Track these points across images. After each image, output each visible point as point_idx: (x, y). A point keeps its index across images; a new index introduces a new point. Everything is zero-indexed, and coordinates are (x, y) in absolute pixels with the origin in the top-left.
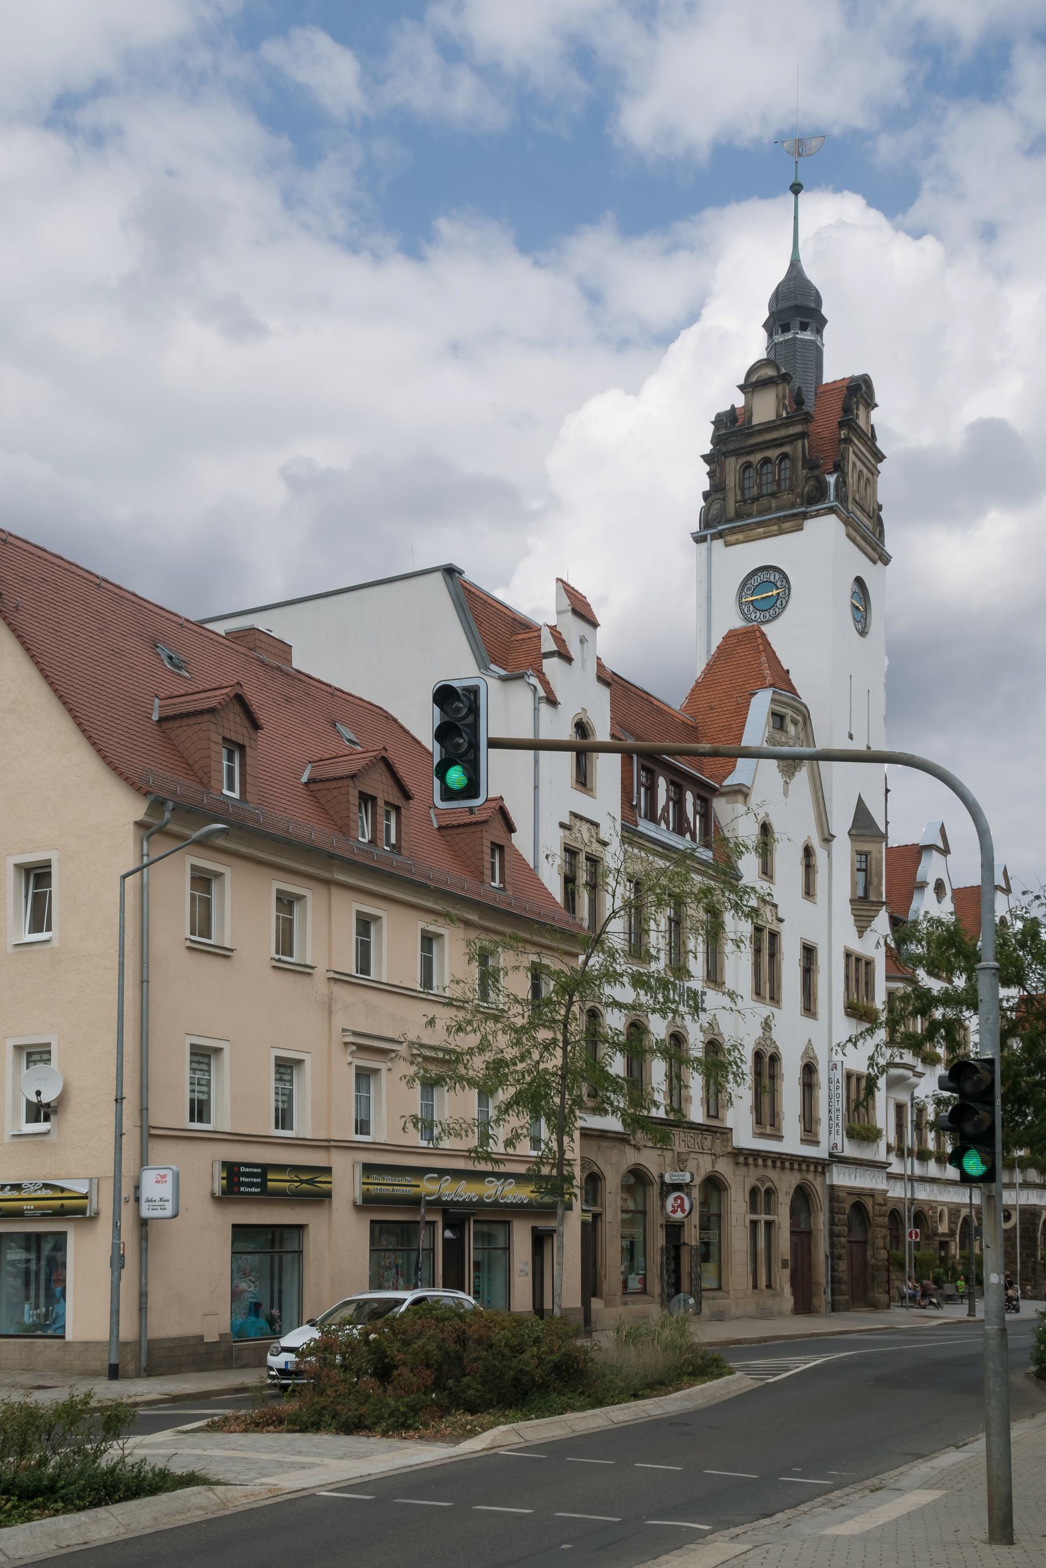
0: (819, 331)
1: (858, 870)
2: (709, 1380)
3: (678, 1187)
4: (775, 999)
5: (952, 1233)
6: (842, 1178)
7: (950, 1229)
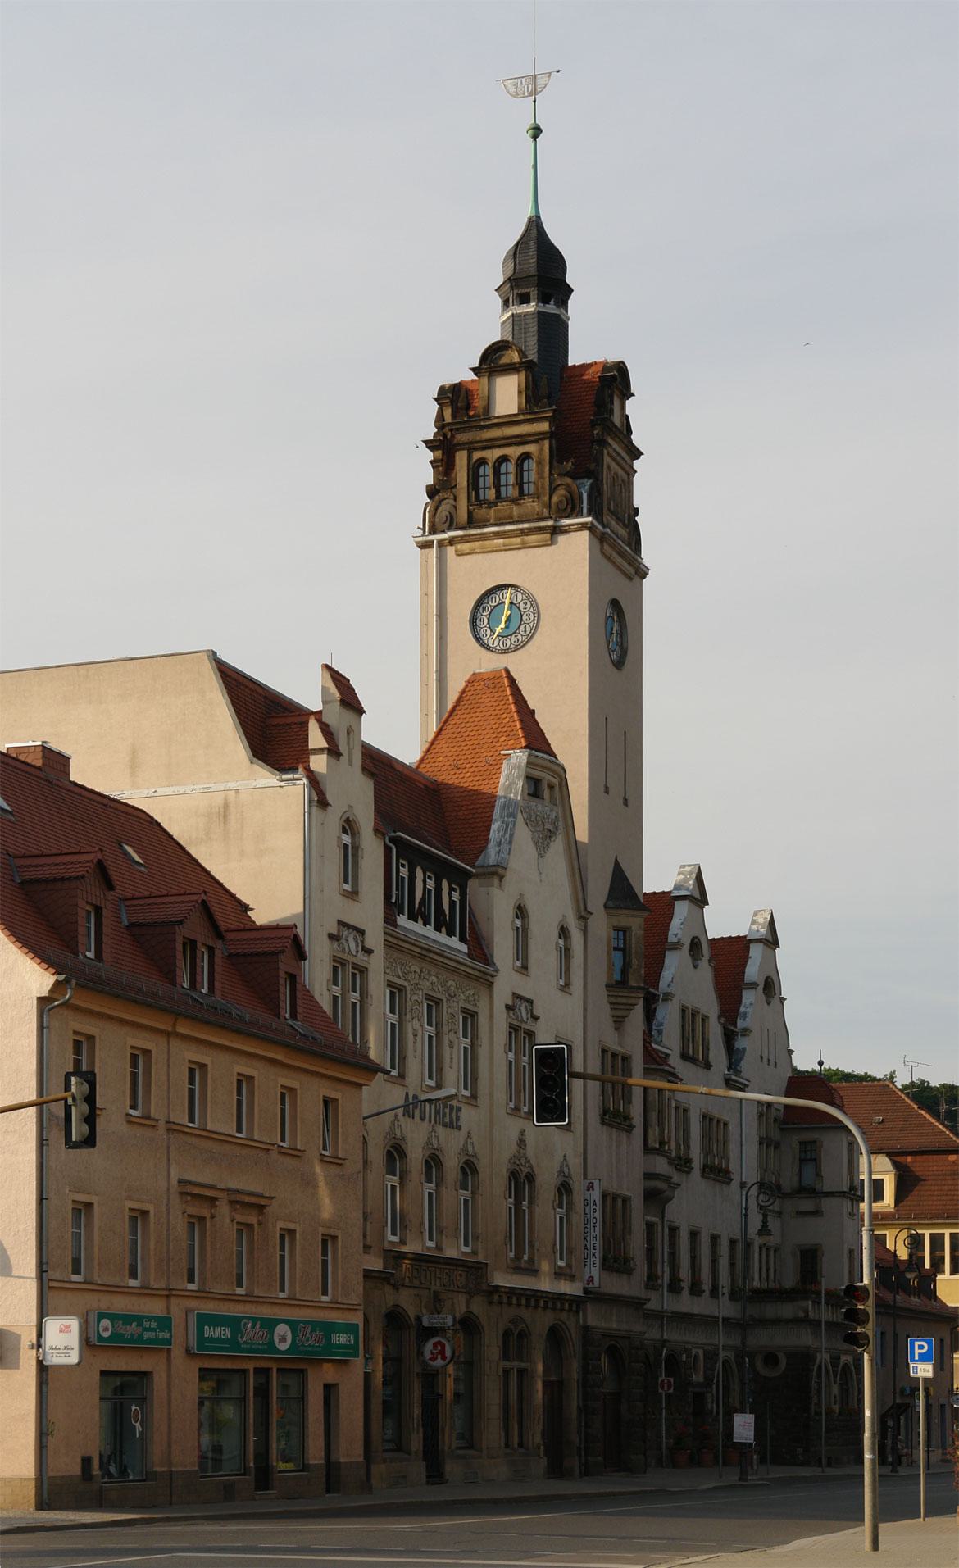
0: (564, 303)
1: (615, 949)
3: (432, 1332)
5: (708, 1381)
6: (593, 1317)
7: (705, 1378)
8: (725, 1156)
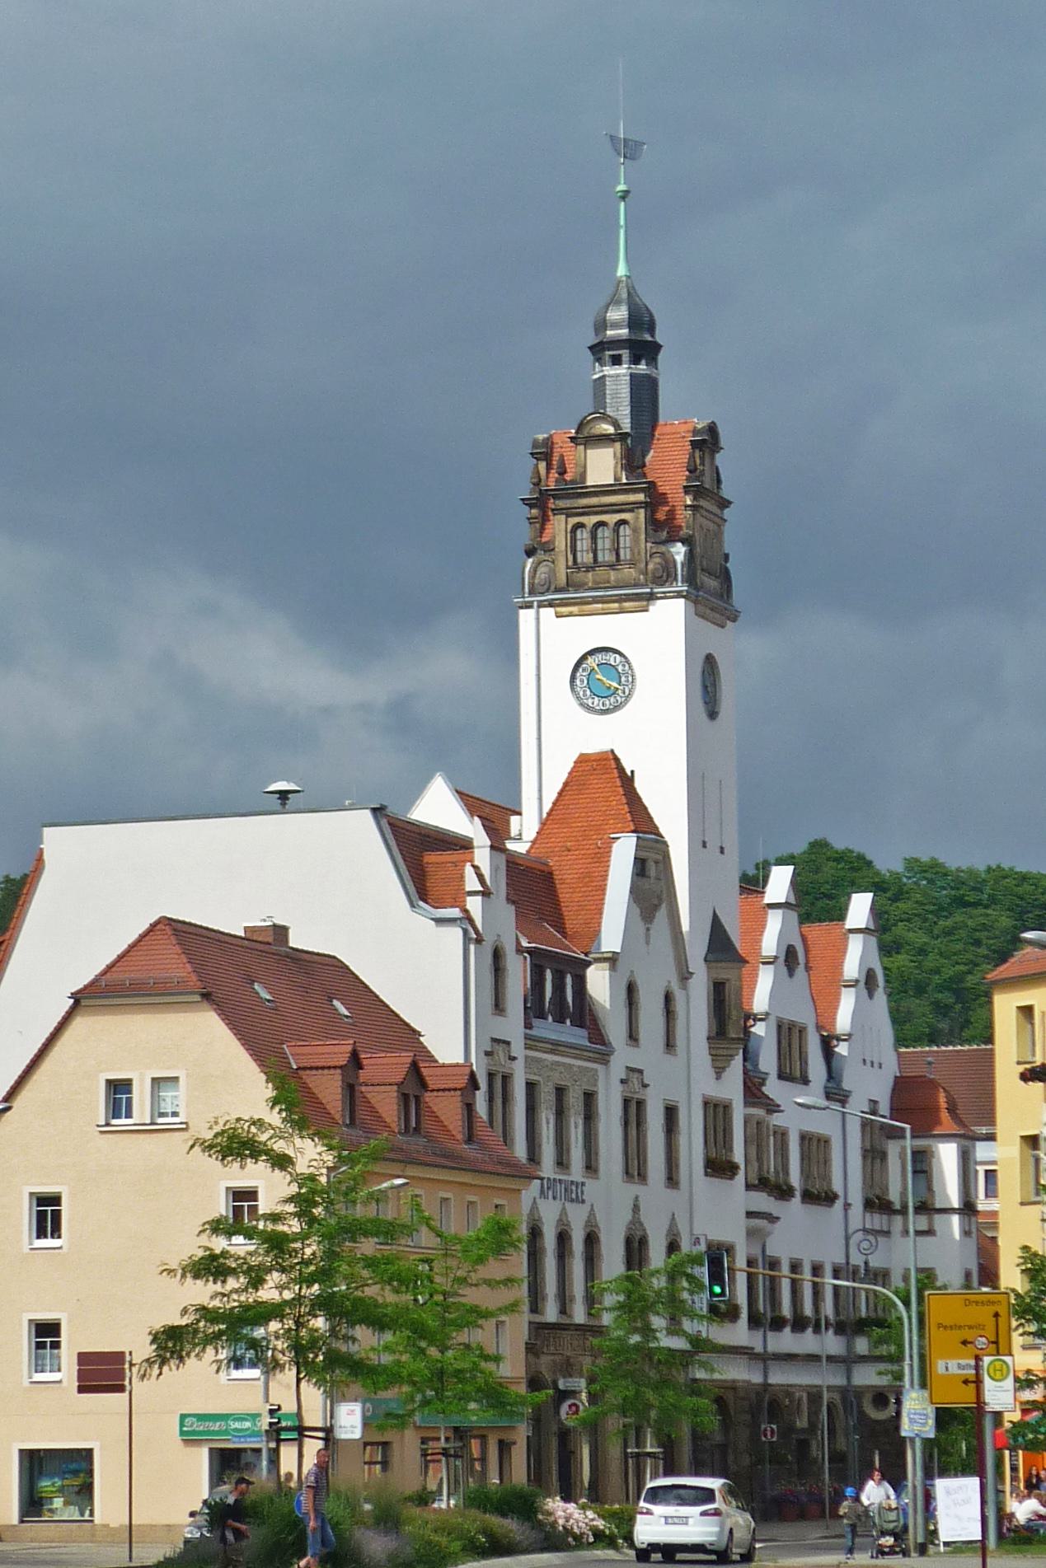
2: (604, 1548)
4: (642, 1177)
8: (826, 1177)
